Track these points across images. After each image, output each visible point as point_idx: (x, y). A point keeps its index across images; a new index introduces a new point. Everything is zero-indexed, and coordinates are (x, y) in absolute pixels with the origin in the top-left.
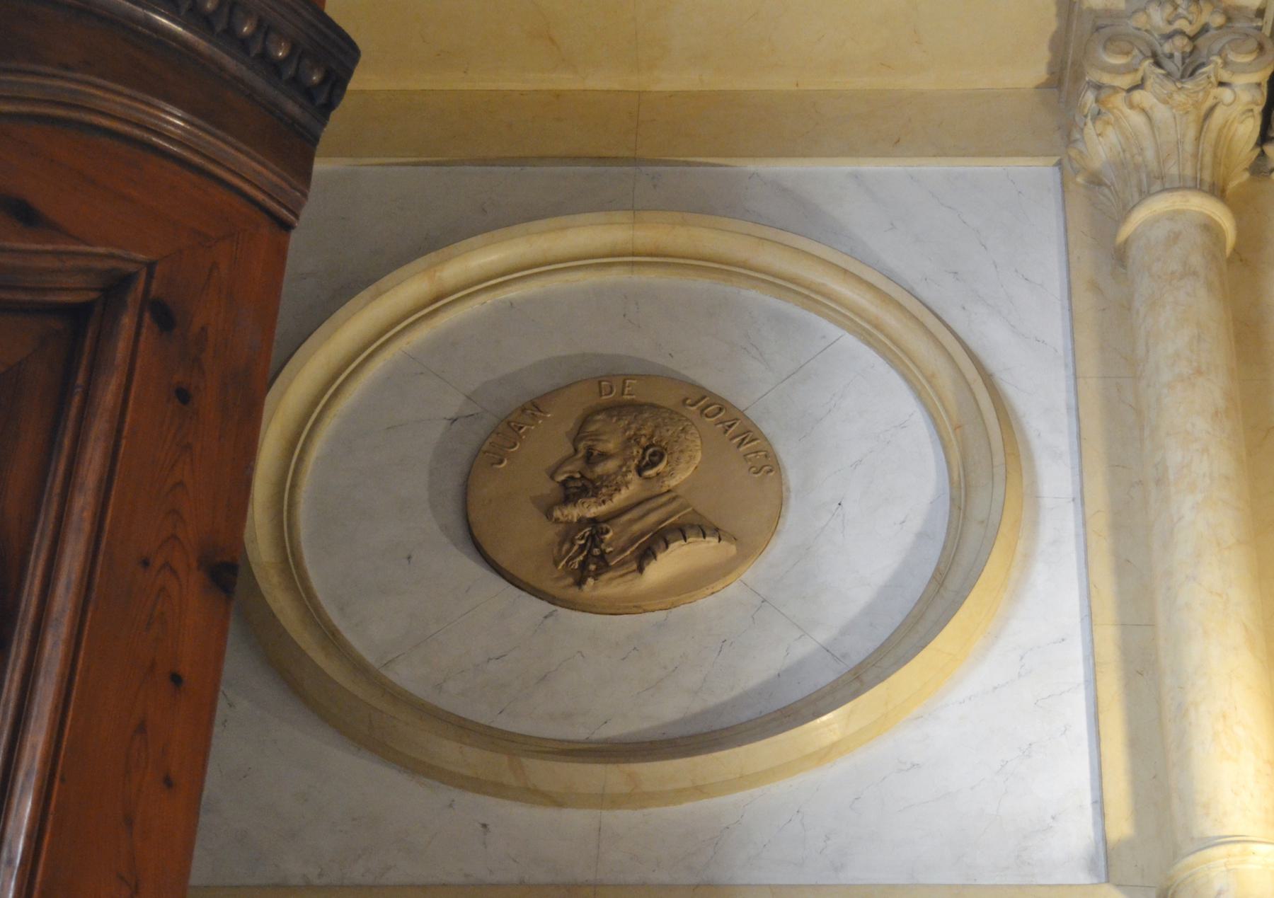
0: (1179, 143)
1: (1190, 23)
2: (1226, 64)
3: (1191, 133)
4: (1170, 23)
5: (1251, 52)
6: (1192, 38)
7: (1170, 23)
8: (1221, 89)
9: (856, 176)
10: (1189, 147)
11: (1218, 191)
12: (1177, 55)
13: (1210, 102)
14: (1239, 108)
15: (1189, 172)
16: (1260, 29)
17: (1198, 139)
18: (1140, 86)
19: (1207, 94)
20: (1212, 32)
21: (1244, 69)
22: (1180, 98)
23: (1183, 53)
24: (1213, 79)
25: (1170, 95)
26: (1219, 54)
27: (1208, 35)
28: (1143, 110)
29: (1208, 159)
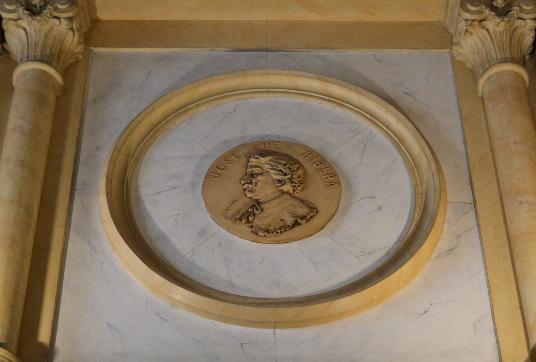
2: (522, 10)
8: (520, 21)
15: (38, 53)
25: (499, 23)
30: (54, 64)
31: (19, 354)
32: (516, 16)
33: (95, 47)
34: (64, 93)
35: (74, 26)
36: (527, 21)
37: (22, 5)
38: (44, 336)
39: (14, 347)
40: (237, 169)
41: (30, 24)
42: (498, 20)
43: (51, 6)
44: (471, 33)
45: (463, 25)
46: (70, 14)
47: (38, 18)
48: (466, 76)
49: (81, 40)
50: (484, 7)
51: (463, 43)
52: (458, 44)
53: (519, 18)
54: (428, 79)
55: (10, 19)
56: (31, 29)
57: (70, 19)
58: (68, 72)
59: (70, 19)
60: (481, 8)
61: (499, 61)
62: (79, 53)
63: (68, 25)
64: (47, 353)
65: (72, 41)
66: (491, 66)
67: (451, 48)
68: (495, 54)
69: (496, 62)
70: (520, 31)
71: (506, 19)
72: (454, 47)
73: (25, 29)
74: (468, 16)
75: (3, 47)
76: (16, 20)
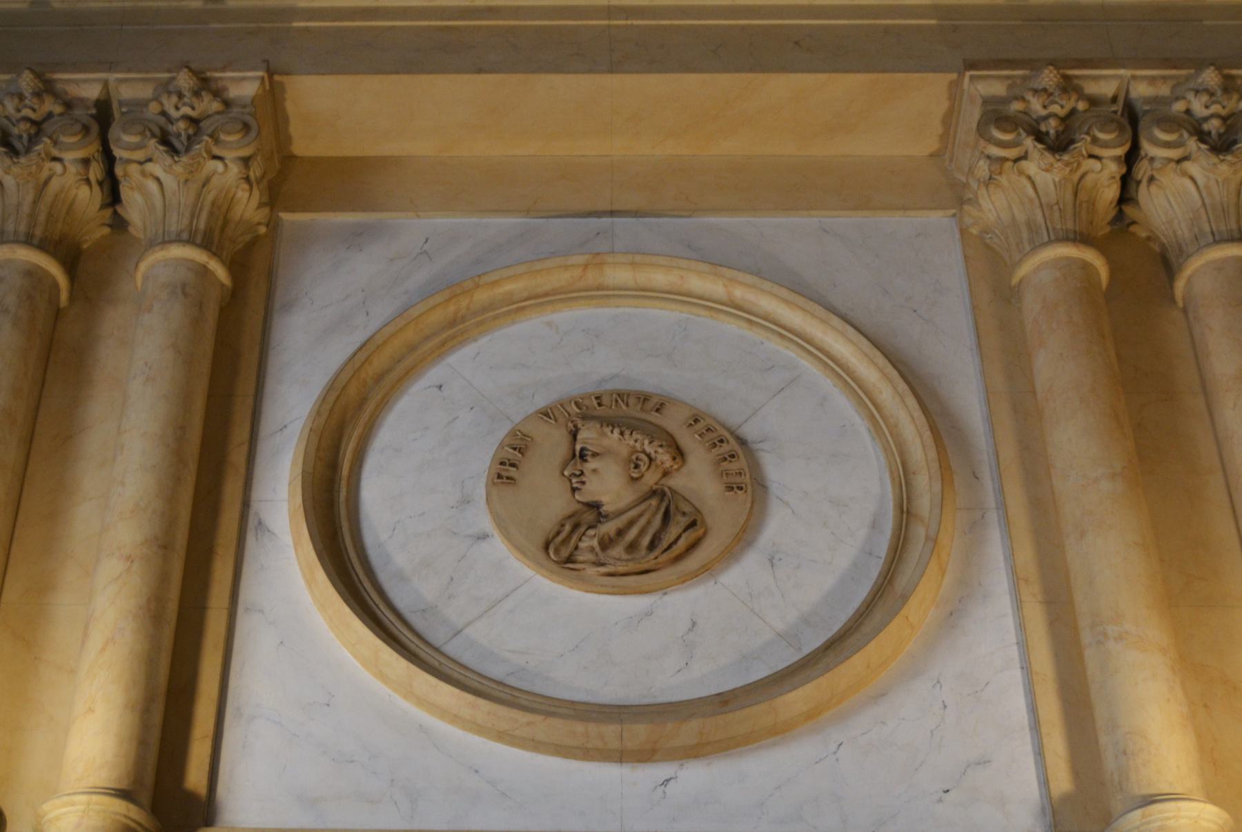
0: (19, 204)
1: (1062, 107)
2: (1095, 141)
3: (30, 198)
4: (19, 110)
5: (75, 134)
6: (1063, 120)
7: (1045, 107)
8: (1092, 161)
9: (549, 324)
10: (26, 208)
11: (1082, 238)
12: (25, 136)
13: (45, 174)
14: (1106, 173)
15: (22, 228)
16: (1115, 112)
17: (35, 202)
18: (1024, 157)
19: (40, 168)
20: (56, 118)
21: (70, 148)
22: (15, 170)
23: (29, 135)
24: (1084, 152)
25: (9, 168)
26: (1088, 133)
27: (53, 120)
28: (1029, 178)
29: (42, 218)
30: (214, 249)
31: (155, 809)
32: (1084, 152)
33: (292, 210)
34: (233, 301)
35: (251, 174)
36: (1104, 161)
37: (153, 135)
38: (195, 778)
39: (146, 797)
40: (553, 441)
41: (168, 170)
42: (1049, 158)
43: (50, 138)
44: (999, 186)
45: (983, 168)
46: (245, 152)
47: (1229, 158)
48: (991, 264)
49: (265, 199)
50: (1186, 135)
51: (985, 202)
52: (974, 202)
53: (1091, 156)
54: (921, 270)
55: (1170, 160)
56: (1209, 179)
57: (246, 161)
58: (239, 265)
59: (246, 161)
60: (1181, 135)
61: (1053, 238)
62: (259, 224)
63: (78, 173)
64: (205, 808)
65: (248, 206)
66: (1050, 242)
67: (961, 209)
68: (175, 223)
69: (1211, 239)
70: (1089, 179)
71: (1066, 157)
72: (966, 207)
73: (158, 180)
74: (995, 151)
75: (115, 213)
76: (1179, 161)
